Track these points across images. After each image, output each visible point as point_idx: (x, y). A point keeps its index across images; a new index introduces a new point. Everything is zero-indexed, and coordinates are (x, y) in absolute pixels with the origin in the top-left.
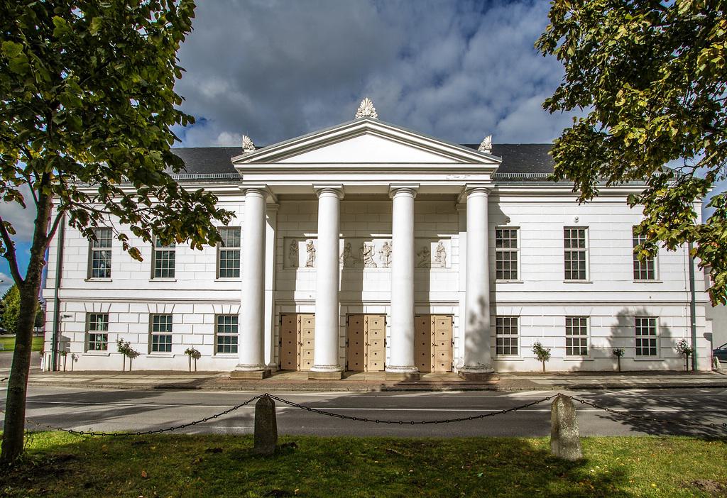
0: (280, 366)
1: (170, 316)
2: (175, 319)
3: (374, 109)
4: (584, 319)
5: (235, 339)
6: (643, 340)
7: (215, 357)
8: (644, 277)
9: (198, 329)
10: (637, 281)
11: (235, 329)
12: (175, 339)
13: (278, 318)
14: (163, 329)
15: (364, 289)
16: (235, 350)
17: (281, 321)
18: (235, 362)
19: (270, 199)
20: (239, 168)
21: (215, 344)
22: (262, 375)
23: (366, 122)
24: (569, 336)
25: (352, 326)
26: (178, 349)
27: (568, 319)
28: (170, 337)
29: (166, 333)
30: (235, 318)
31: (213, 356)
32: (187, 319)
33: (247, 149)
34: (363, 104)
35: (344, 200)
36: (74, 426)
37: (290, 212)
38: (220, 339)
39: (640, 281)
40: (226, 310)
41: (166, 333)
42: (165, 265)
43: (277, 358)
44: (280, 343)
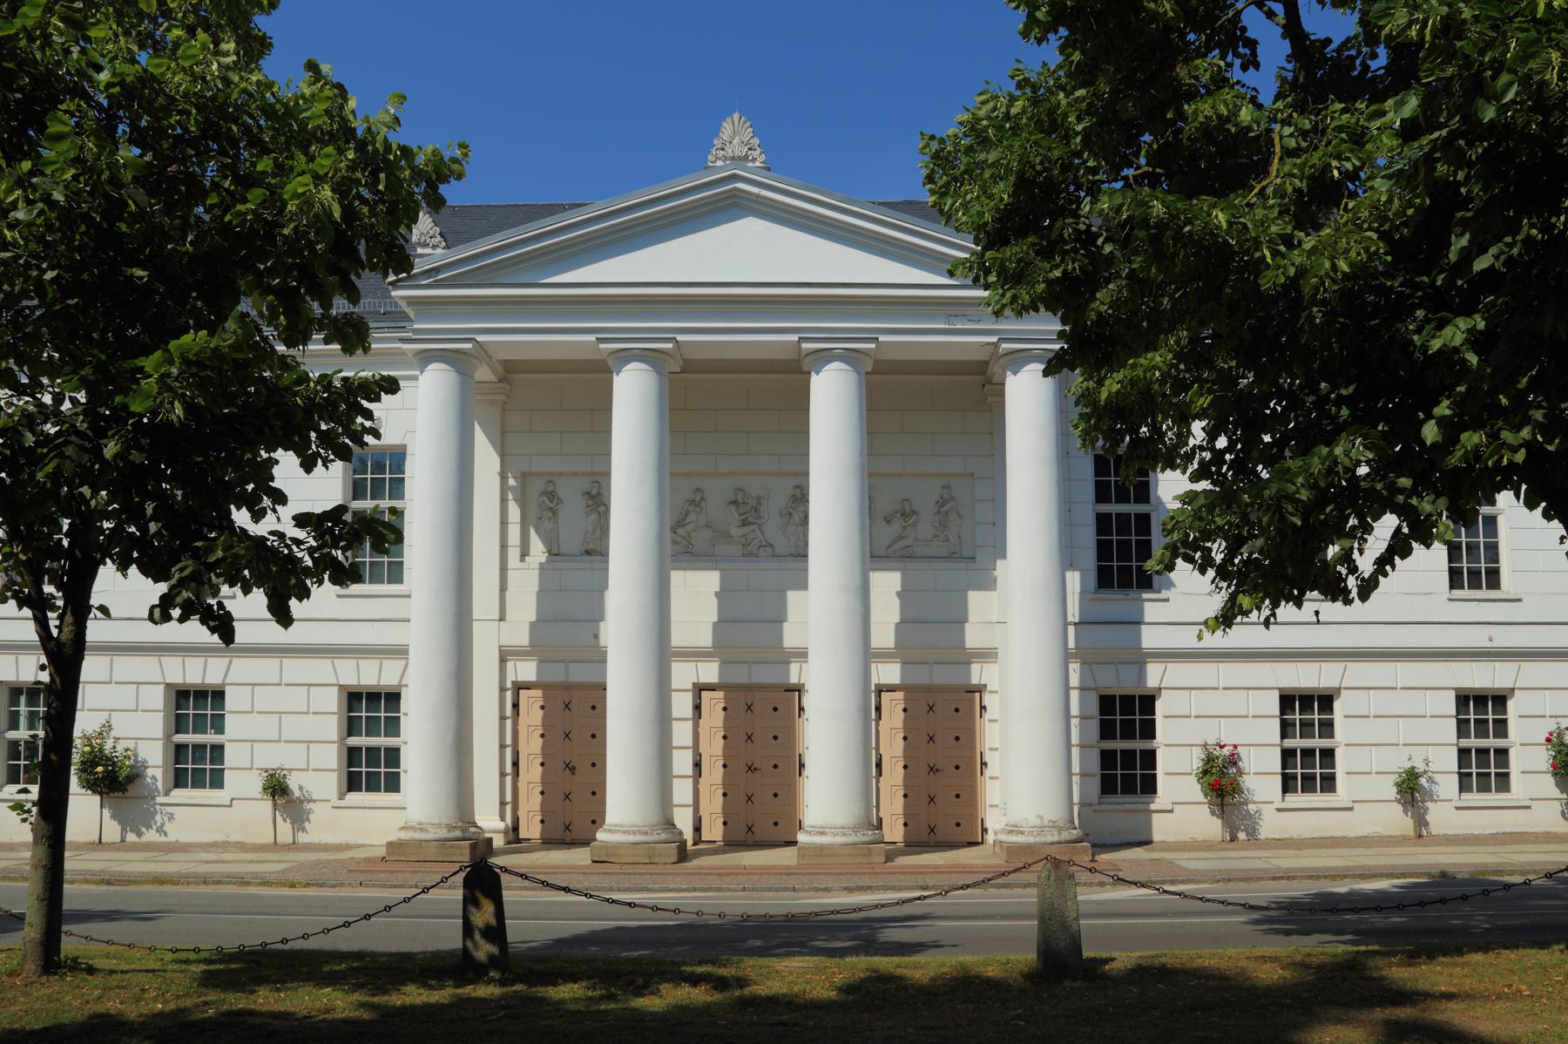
0: (516, 829)
1: (219, 695)
2: (234, 699)
3: (756, 141)
4: (1500, 700)
5: (393, 756)
6: (1321, 751)
7: (342, 803)
8: (1475, 584)
9: (293, 726)
10: (1457, 593)
11: (393, 727)
12: (231, 757)
13: (509, 694)
14: (1128, 734)
15: (972, 616)
16: (393, 784)
17: (516, 706)
18: (398, 819)
19: (484, 373)
20: (403, 298)
21: (339, 770)
22: (467, 851)
23: (735, 178)
24: (1464, 743)
25: (937, 727)
26: (243, 781)
27: (1463, 699)
28: (218, 750)
29: (1138, 745)
30: (393, 698)
31: (335, 801)
32: (265, 699)
33: (426, 245)
34: (727, 127)
35: (873, 373)
36: (707, 1008)
37: (540, 412)
38: (352, 754)
39: (1465, 593)
40: (369, 675)
41: (209, 738)
42: (1124, 546)
43: (509, 808)
44: (515, 764)
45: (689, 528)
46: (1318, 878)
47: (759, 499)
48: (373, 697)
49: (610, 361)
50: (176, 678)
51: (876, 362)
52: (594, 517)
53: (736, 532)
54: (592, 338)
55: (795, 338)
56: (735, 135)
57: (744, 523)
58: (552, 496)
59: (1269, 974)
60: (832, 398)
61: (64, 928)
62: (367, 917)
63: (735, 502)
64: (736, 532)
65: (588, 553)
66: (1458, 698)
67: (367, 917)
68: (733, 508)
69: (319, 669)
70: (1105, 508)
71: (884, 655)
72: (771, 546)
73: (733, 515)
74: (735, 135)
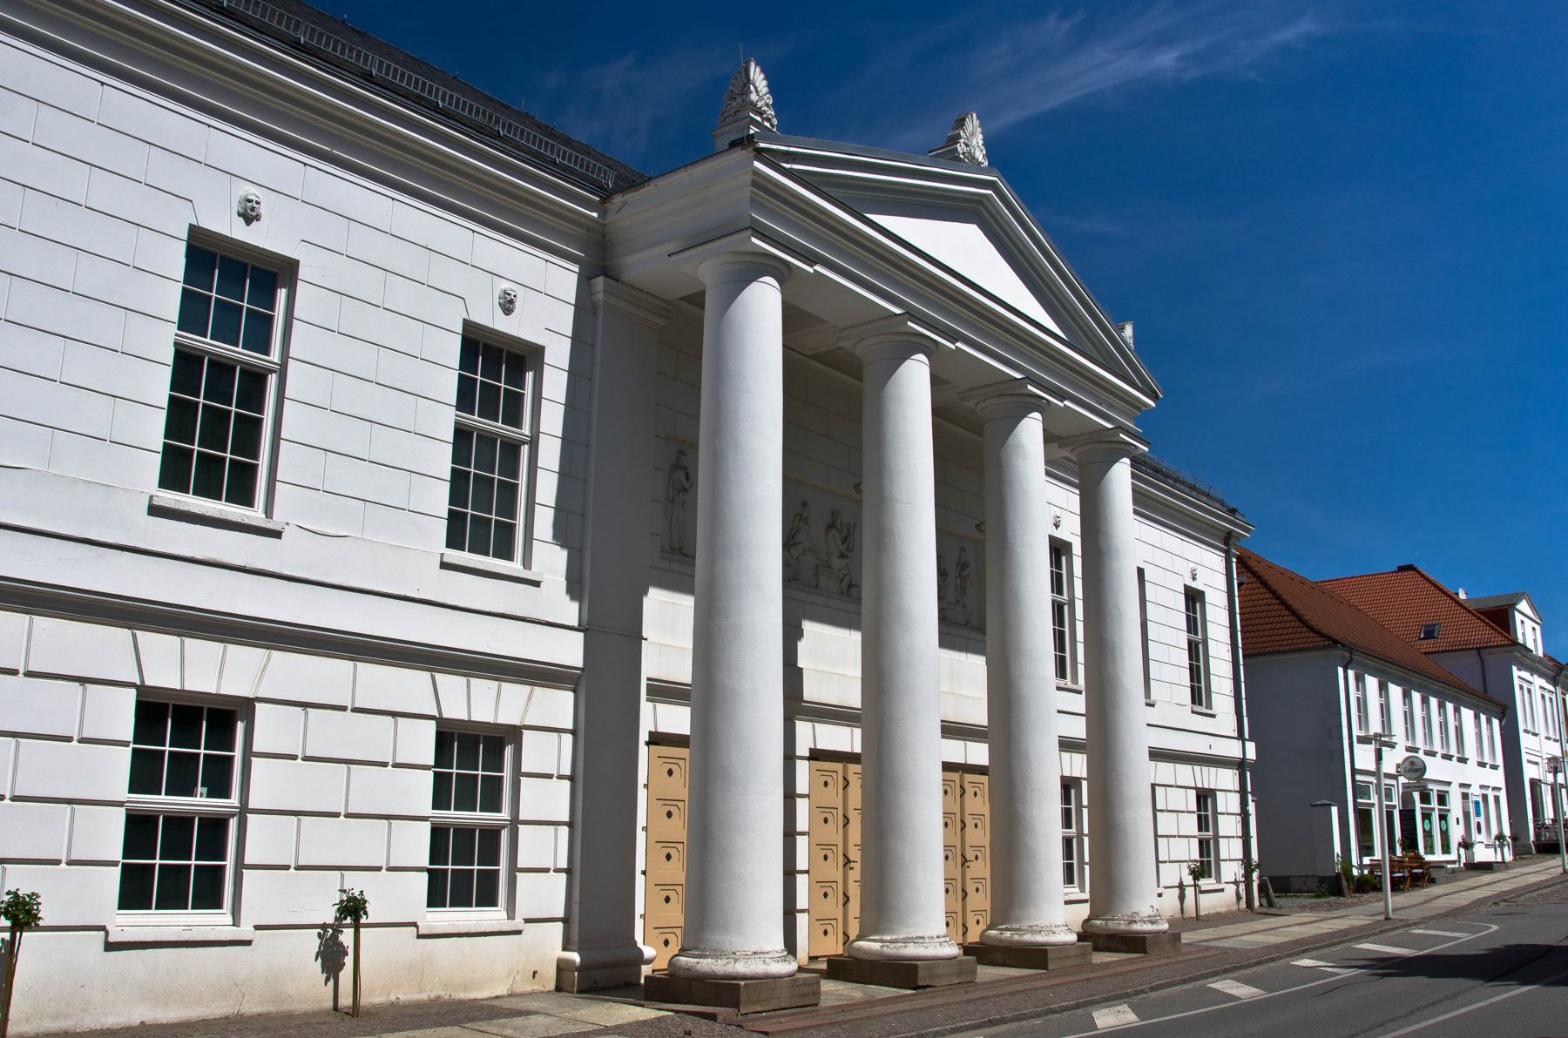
2: (270, 728)
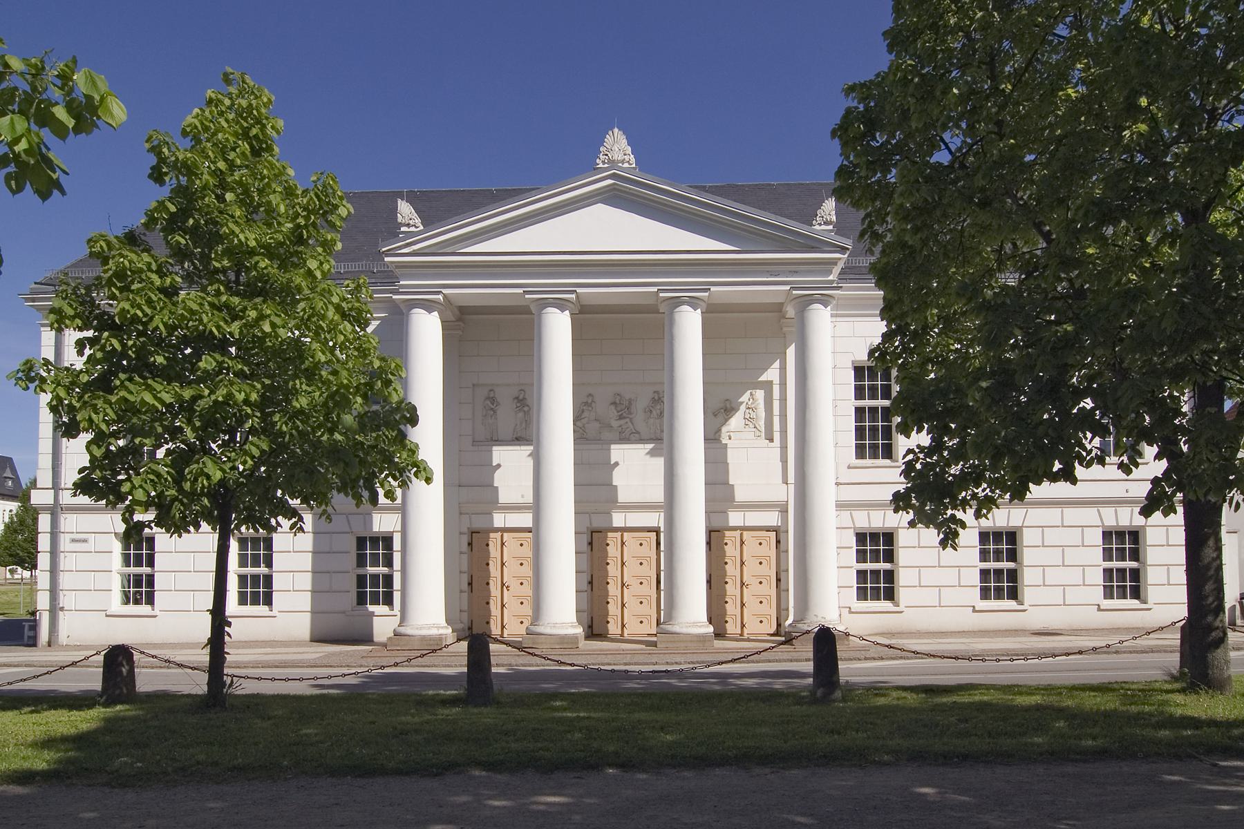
2: (1028, 538)
32: (1052, 536)
39: (868, 462)
45: (584, 421)
46: (1069, 654)
47: (630, 401)
48: (874, 536)
49: (402, 306)
50: (1110, 522)
51: (709, 305)
52: (521, 415)
53: (615, 424)
54: (520, 291)
55: (655, 289)
56: (617, 147)
57: (621, 417)
58: (493, 400)
59: (93, 725)
60: (558, 329)
61: (465, 669)
62: (62, 668)
63: (614, 403)
64: (615, 424)
65: (517, 439)
66: (857, 535)
67: (62, 668)
68: (613, 407)
69: (1088, 515)
70: (861, 403)
71: (45, 508)
72: (638, 433)
73: (613, 413)
74: (617, 147)
